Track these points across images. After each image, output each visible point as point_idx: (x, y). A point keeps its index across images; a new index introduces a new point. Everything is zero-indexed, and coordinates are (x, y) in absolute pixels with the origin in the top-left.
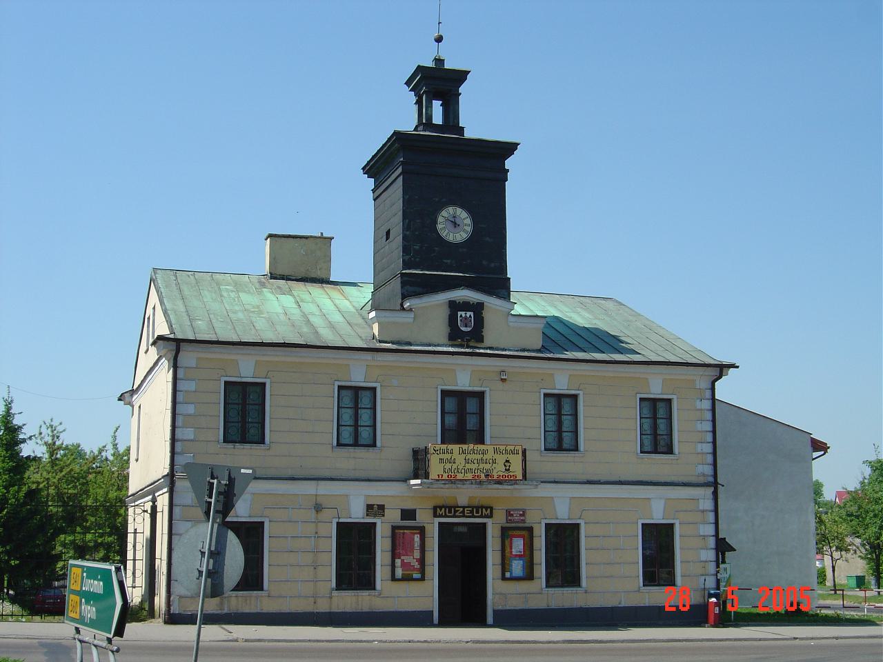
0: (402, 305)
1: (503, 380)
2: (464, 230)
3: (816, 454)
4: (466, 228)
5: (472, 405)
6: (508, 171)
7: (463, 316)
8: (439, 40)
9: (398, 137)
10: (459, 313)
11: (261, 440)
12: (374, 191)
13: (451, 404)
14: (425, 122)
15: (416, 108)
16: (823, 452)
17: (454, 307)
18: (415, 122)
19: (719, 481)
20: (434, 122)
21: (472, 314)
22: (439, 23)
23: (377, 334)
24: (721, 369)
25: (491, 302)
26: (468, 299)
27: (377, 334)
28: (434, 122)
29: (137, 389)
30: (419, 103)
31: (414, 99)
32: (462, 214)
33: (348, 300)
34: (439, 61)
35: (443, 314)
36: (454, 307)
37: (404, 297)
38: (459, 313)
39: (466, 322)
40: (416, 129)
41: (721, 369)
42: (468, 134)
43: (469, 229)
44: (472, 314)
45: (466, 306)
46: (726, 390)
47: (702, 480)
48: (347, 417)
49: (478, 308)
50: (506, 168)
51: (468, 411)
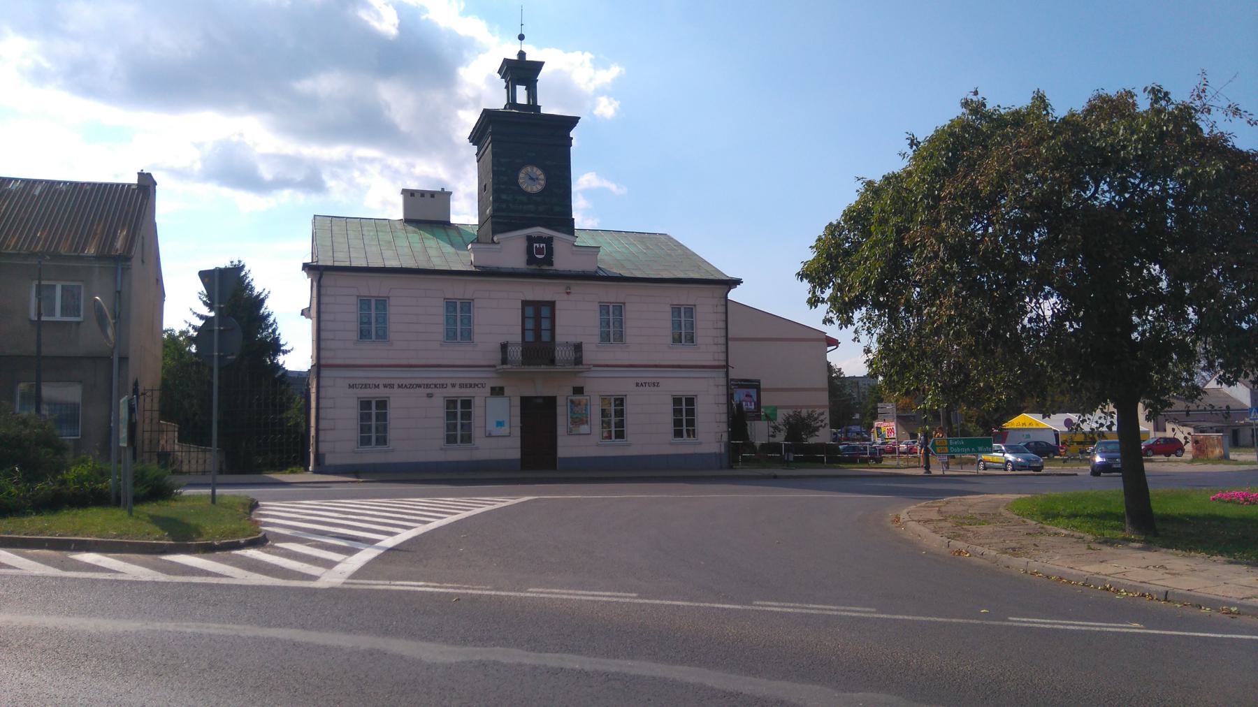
0: (493, 239)
1: (568, 293)
2: (539, 184)
3: (829, 349)
4: (529, 188)
5: (545, 312)
6: (572, 138)
7: (538, 246)
8: (521, 37)
9: (526, 89)
10: (535, 245)
11: (574, 388)
12: (477, 155)
13: (530, 311)
14: (512, 102)
15: (505, 90)
16: (835, 347)
17: (531, 240)
18: (506, 103)
19: (730, 364)
20: (518, 101)
21: (544, 245)
22: (522, 25)
23: (473, 260)
24: (736, 282)
25: (559, 237)
26: (540, 235)
27: (473, 260)
28: (518, 101)
29: (757, 400)
30: (507, 87)
31: (505, 84)
32: (538, 172)
33: (462, 237)
34: (522, 54)
35: (523, 245)
36: (531, 240)
37: (495, 232)
38: (535, 245)
39: (540, 251)
40: (505, 108)
41: (736, 282)
42: (543, 111)
43: (542, 182)
44: (544, 245)
45: (540, 239)
46: (734, 295)
47: (716, 363)
48: (530, 324)
49: (549, 241)
50: (571, 136)
51: (542, 316)
